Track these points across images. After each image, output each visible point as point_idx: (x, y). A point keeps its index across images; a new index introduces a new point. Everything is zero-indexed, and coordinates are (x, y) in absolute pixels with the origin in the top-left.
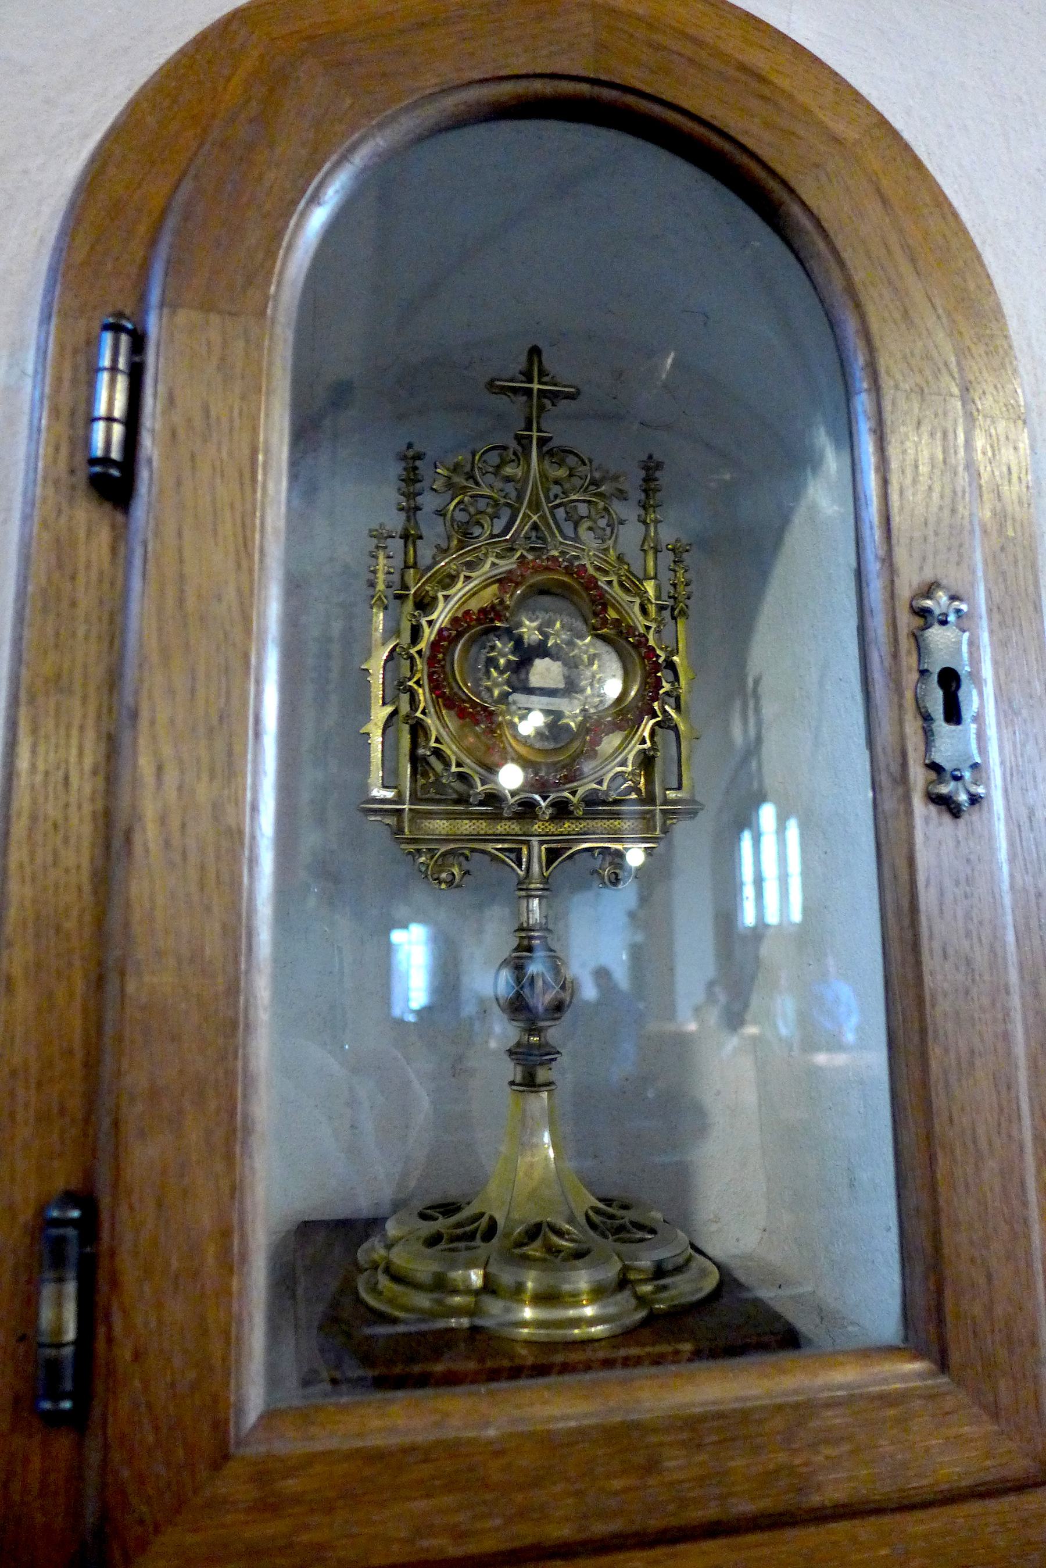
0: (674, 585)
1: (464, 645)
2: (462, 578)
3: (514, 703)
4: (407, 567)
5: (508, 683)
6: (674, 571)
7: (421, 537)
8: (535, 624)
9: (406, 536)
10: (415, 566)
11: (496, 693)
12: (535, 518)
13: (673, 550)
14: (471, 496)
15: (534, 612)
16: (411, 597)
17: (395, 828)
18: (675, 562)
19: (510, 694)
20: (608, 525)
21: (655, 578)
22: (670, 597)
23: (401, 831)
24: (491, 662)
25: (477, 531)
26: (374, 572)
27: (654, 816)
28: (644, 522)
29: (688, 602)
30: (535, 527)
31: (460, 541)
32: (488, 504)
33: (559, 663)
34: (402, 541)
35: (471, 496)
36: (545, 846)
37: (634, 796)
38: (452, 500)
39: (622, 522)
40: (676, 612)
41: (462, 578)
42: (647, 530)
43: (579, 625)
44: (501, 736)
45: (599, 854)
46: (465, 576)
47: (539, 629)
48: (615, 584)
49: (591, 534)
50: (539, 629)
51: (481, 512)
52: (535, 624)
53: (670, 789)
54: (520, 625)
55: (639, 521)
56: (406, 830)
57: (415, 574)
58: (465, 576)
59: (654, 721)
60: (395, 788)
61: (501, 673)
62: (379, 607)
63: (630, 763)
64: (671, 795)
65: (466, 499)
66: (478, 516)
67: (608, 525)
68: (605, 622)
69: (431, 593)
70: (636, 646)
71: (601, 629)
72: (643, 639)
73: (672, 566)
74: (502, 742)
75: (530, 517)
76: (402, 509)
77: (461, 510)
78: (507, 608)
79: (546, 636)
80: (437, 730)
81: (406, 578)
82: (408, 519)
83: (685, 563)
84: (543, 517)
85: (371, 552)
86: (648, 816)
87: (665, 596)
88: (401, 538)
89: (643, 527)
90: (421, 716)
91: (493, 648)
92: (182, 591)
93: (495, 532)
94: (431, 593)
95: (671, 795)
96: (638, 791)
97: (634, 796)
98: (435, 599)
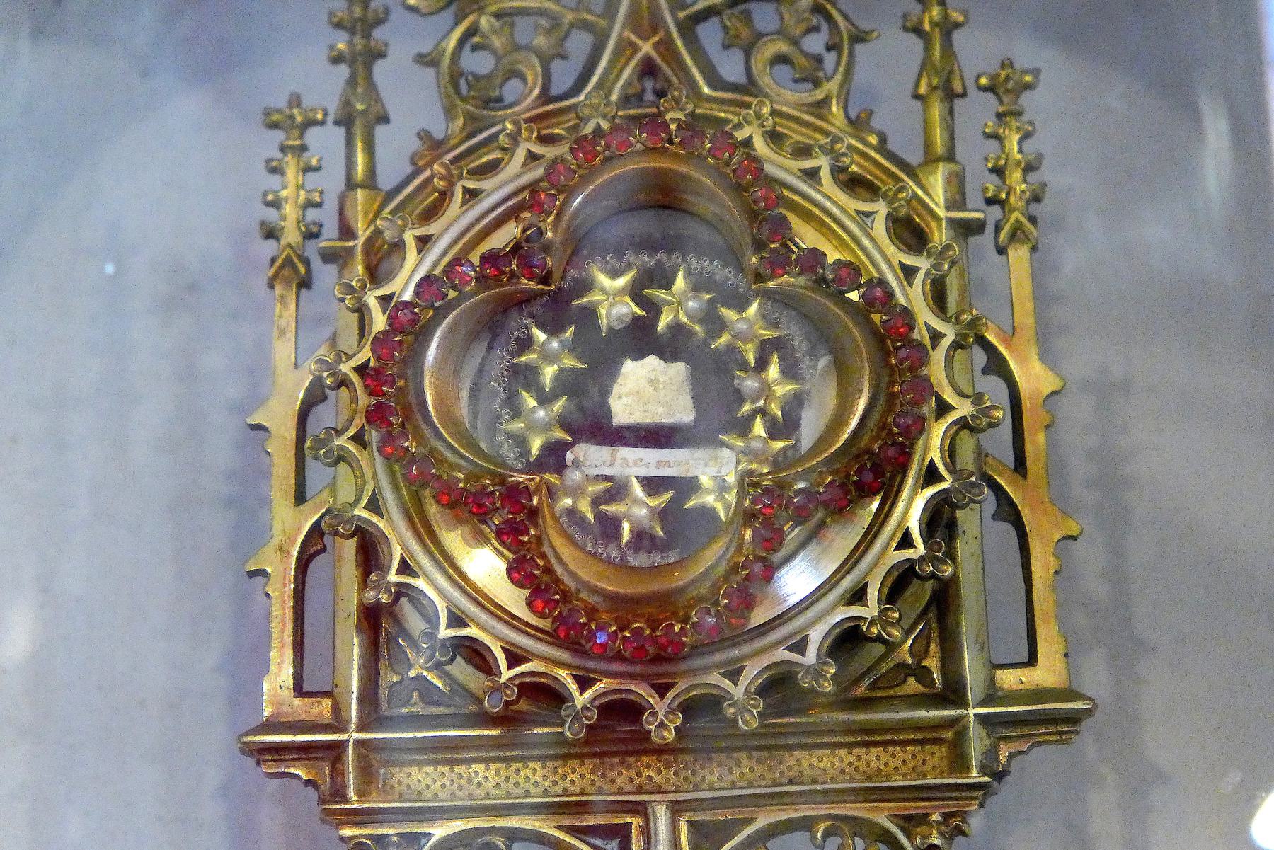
0: (999, 171)
1: (445, 338)
2: (459, 195)
3: (577, 464)
4: (351, 185)
5: (563, 423)
6: (995, 136)
7: (384, 119)
8: (622, 282)
9: (346, 121)
10: (370, 182)
11: (536, 445)
12: (646, 48)
13: (991, 89)
14: (498, 16)
15: (620, 255)
16: (359, 255)
17: (326, 788)
18: (1000, 116)
19: (568, 446)
20: (829, 48)
21: (950, 157)
22: (990, 202)
23: (339, 794)
24: (525, 377)
25: (512, 89)
26: (276, 204)
27: (962, 734)
28: (918, 31)
29: (1034, 208)
30: (648, 69)
31: (470, 118)
32: (536, 27)
33: (679, 369)
34: (341, 131)
35: (498, 16)
36: (688, 816)
37: (912, 686)
38: (457, 24)
39: (859, 38)
40: (1003, 234)
41: (459, 195)
42: (928, 48)
43: (719, 271)
44: (539, 539)
45: (826, 835)
46: (467, 191)
47: (635, 293)
48: (825, 174)
49: (784, 71)
50: (635, 293)
51: (518, 48)
52: (622, 282)
53: (1002, 666)
54: (586, 286)
55: (905, 29)
56: (351, 793)
57: (369, 202)
58: (467, 191)
59: (931, 490)
60: (327, 694)
61: (544, 399)
62: (287, 283)
63: (872, 593)
64: (1009, 679)
65: (484, 22)
66: (516, 56)
67: (829, 48)
68: (780, 263)
69: (388, 235)
70: (861, 313)
71: (774, 275)
72: (879, 292)
73: (991, 126)
74: (543, 556)
75: (635, 48)
76: (337, 60)
77: (475, 48)
78: (546, 248)
79: (653, 309)
80: (405, 547)
81: (349, 213)
82: (352, 82)
83: (1026, 117)
84: (666, 46)
85: (268, 161)
86: (949, 735)
87: (974, 198)
88: (337, 123)
89: (916, 43)
90: (366, 514)
91: (526, 343)
92: (399, 534)
93: (554, 91)
94: (388, 235)
95: (1009, 679)
96: (923, 674)
97: (912, 686)
98: (399, 246)
